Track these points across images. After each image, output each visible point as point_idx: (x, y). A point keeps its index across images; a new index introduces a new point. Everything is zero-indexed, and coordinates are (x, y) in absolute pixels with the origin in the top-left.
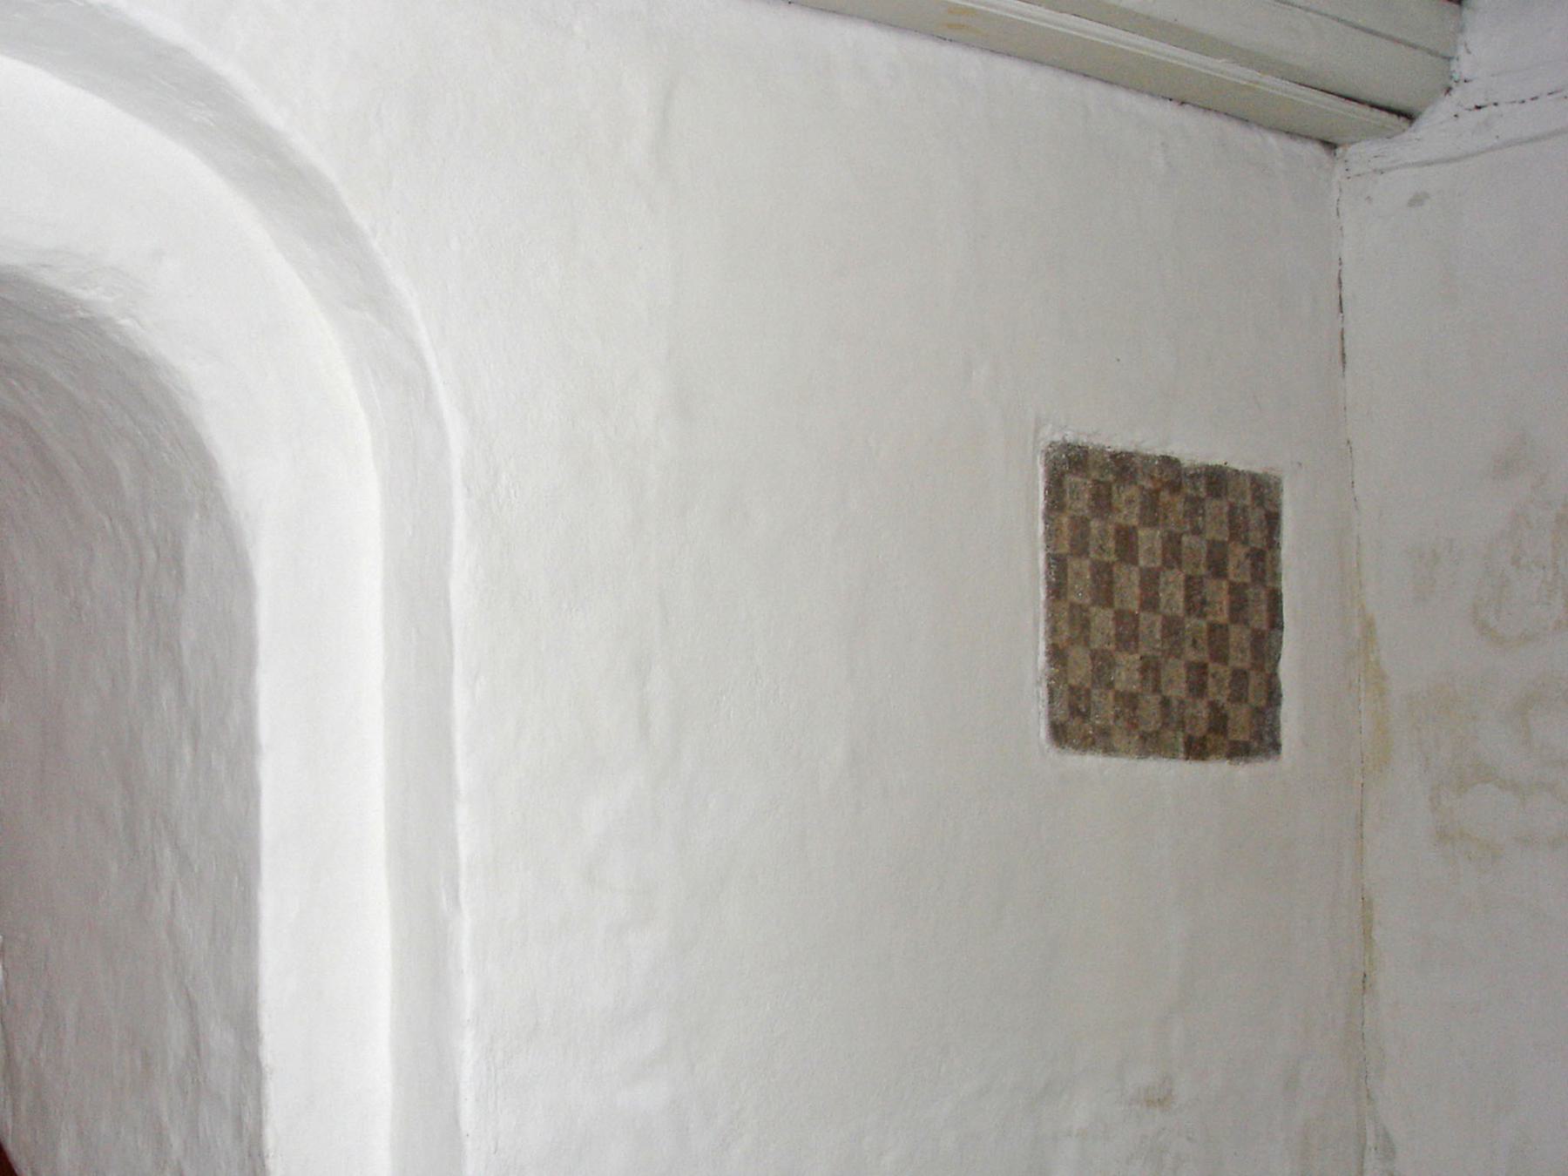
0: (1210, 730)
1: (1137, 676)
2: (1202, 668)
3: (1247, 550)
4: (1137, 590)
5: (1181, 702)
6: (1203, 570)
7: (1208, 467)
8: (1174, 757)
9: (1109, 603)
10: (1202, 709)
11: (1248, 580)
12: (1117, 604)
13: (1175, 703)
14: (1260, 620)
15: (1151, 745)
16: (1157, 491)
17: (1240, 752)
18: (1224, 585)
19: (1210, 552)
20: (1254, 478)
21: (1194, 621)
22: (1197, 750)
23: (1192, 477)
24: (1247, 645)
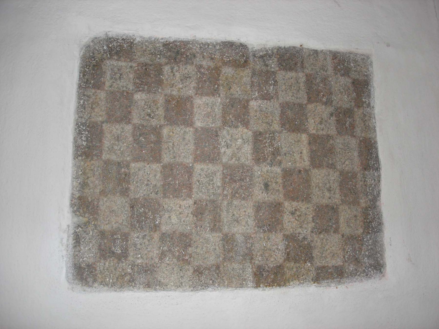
0: (288, 258)
1: (191, 218)
2: (277, 207)
3: (330, 109)
4: (192, 147)
5: (247, 237)
6: (276, 126)
7: (279, 49)
8: (242, 286)
9: (156, 157)
10: (277, 241)
11: (333, 131)
12: (166, 158)
13: (240, 238)
14: (351, 161)
15: (207, 276)
16: (217, 69)
17: (361, 87)
18: (304, 137)
19: (283, 113)
20: (335, 55)
21: (265, 168)
22: (270, 276)
23: (262, 57)
24: (335, 186)
